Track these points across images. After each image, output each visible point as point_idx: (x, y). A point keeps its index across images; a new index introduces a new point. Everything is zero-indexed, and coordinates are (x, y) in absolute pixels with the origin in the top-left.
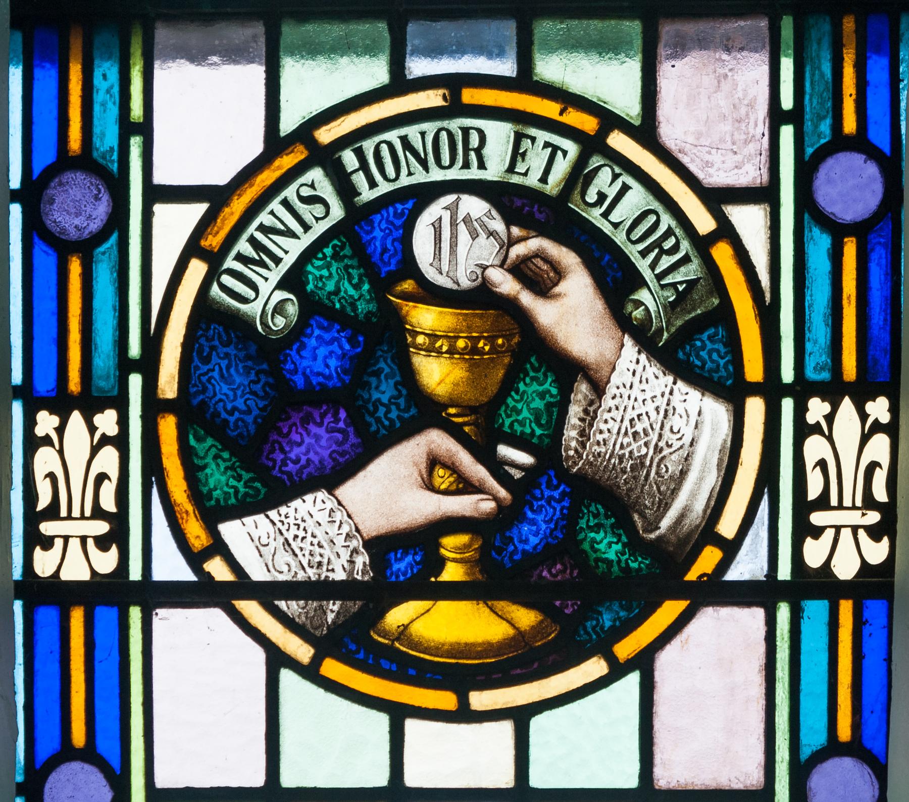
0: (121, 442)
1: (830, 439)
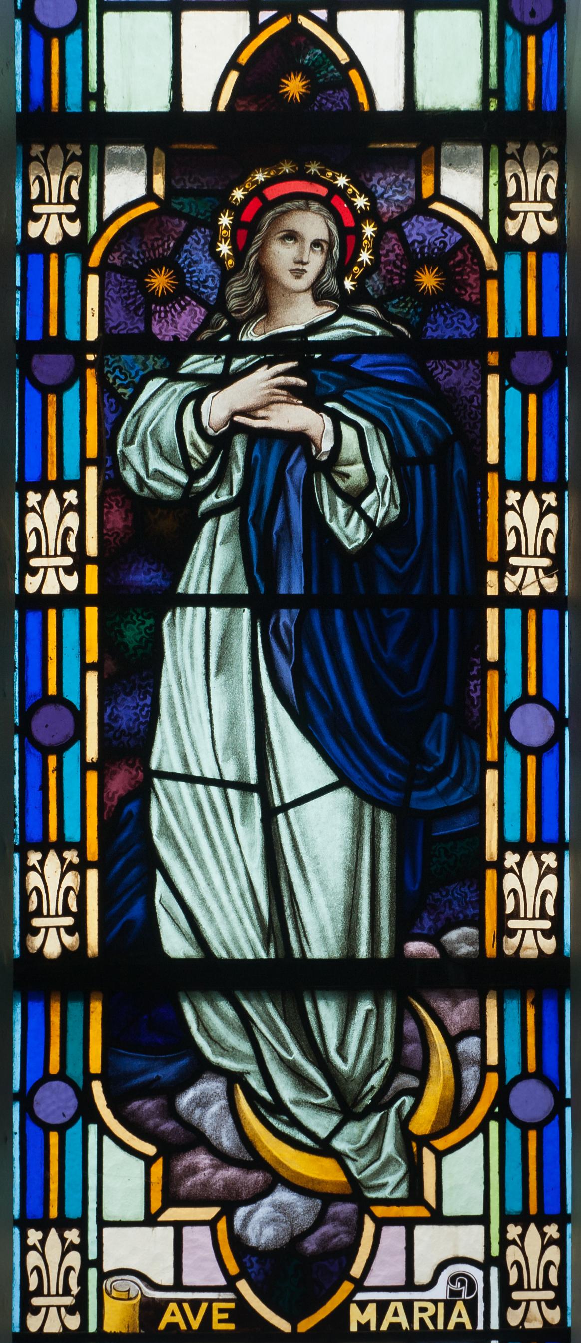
0: (81, 509)
1: (522, 1249)
